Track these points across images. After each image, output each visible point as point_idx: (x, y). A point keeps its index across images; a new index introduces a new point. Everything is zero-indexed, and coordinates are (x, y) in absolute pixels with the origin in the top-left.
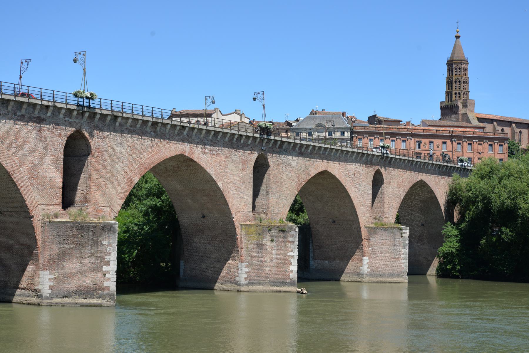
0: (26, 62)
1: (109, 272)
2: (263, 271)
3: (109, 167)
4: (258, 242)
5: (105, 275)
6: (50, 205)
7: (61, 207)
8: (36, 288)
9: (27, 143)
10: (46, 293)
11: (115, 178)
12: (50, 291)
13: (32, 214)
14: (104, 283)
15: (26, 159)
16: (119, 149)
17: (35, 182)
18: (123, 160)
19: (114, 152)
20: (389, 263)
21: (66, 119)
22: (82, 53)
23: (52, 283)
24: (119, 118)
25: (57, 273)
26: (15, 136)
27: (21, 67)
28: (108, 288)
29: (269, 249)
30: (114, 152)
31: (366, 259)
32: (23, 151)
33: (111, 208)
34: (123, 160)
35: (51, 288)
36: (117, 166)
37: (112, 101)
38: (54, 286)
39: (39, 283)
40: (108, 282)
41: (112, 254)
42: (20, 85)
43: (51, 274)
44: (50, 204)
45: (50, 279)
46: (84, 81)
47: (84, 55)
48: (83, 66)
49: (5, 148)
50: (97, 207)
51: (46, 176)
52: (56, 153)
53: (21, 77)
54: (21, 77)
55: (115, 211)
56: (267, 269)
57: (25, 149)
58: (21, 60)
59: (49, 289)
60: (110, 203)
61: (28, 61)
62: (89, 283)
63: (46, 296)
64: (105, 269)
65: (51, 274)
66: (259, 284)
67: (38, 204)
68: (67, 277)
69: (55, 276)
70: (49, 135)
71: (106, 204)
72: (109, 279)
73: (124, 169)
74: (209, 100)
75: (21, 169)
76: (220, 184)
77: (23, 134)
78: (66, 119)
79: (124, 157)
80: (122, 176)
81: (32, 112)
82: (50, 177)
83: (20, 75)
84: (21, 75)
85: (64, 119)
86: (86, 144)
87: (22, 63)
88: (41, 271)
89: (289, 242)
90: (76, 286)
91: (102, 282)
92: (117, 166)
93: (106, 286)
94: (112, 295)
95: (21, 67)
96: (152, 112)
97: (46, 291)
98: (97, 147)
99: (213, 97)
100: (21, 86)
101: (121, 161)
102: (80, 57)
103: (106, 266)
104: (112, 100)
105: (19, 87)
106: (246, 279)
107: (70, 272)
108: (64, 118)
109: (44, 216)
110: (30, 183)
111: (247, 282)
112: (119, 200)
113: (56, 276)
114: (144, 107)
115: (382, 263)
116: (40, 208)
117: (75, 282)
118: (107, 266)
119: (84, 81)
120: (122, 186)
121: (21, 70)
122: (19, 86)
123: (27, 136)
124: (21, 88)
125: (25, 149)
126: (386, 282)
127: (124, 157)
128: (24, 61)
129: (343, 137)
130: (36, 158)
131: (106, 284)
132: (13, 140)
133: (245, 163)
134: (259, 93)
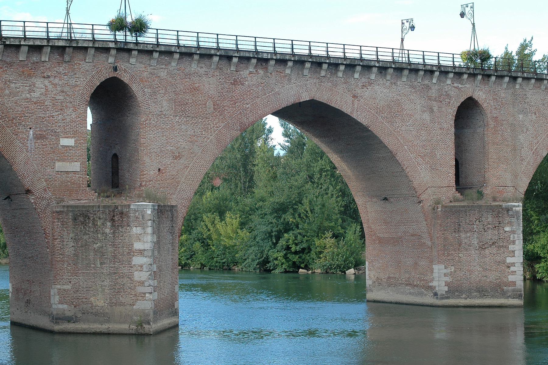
0: (407, 22)
1: (513, 264)
3: (511, 139)
6: (442, 187)
7: (454, 190)
8: (430, 284)
9: (411, 116)
10: (441, 290)
11: (518, 151)
12: (446, 289)
14: (509, 277)
15: (411, 135)
16: (521, 116)
17: (422, 161)
18: (527, 130)
19: (515, 120)
21: (456, 85)
22: (469, 6)
23: (448, 279)
24: (519, 79)
25: (453, 267)
26: (396, 109)
27: (402, 28)
28: (514, 283)
30: (515, 120)
32: (407, 125)
33: (515, 189)
34: (527, 130)
35: (447, 284)
36: (520, 137)
37: (438, 53)
38: (452, 282)
39: (432, 280)
40: (514, 276)
41: (517, 242)
42: (402, 50)
43: (446, 268)
44: (441, 186)
45: (445, 275)
46: (474, 37)
47: (472, 7)
48: (472, 20)
49: (386, 123)
50: (497, 187)
51: (435, 154)
52: (445, 126)
53: (402, 40)
54: (402, 40)
55: (520, 191)
57: (409, 123)
58: (402, 20)
59: (445, 286)
60: (513, 182)
61: (410, 20)
62: (492, 277)
63: (442, 294)
64: (509, 260)
65: (446, 268)
67: (428, 186)
68: (465, 271)
69: (451, 271)
70: (435, 105)
71: (509, 183)
72: (514, 272)
73: (529, 140)
74: (407, 25)
75: (406, 147)
77: (406, 106)
78: (456, 85)
79: (528, 125)
80: (526, 148)
81: (415, 79)
82: (440, 155)
83: (402, 38)
84: (403, 38)
85: (453, 85)
86: (481, 113)
87: (403, 23)
88: (435, 264)
90: (476, 282)
91: (506, 277)
92: (520, 137)
93: (511, 280)
95: (402, 28)
96: (424, 57)
98: (494, 116)
99: (412, 20)
100: (403, 50)
101: (525, 130)
102: (467, 10)
103: (510, 257)
104: (327, 43)
105: (401, 52)
107: (468, 265)
108: (453, 84)
110: (416, 163)
112: (524, 178)
113: (452, 271)
114: (159, 32)
116: (429, 191)
117: (474, 277)
118: (511, 257)
119: (474, 37)
120: (527, 160)
121: (402, 32)
122: (401, 50)
123: (410, 108)
124: (403, 52)
125: (409, 123)
126: (458, 307)
127: (528, 125)
128: (405, 21)
130: (422, 132)
131: (511, 278)
132: (394, 113)
134: (467, 6)
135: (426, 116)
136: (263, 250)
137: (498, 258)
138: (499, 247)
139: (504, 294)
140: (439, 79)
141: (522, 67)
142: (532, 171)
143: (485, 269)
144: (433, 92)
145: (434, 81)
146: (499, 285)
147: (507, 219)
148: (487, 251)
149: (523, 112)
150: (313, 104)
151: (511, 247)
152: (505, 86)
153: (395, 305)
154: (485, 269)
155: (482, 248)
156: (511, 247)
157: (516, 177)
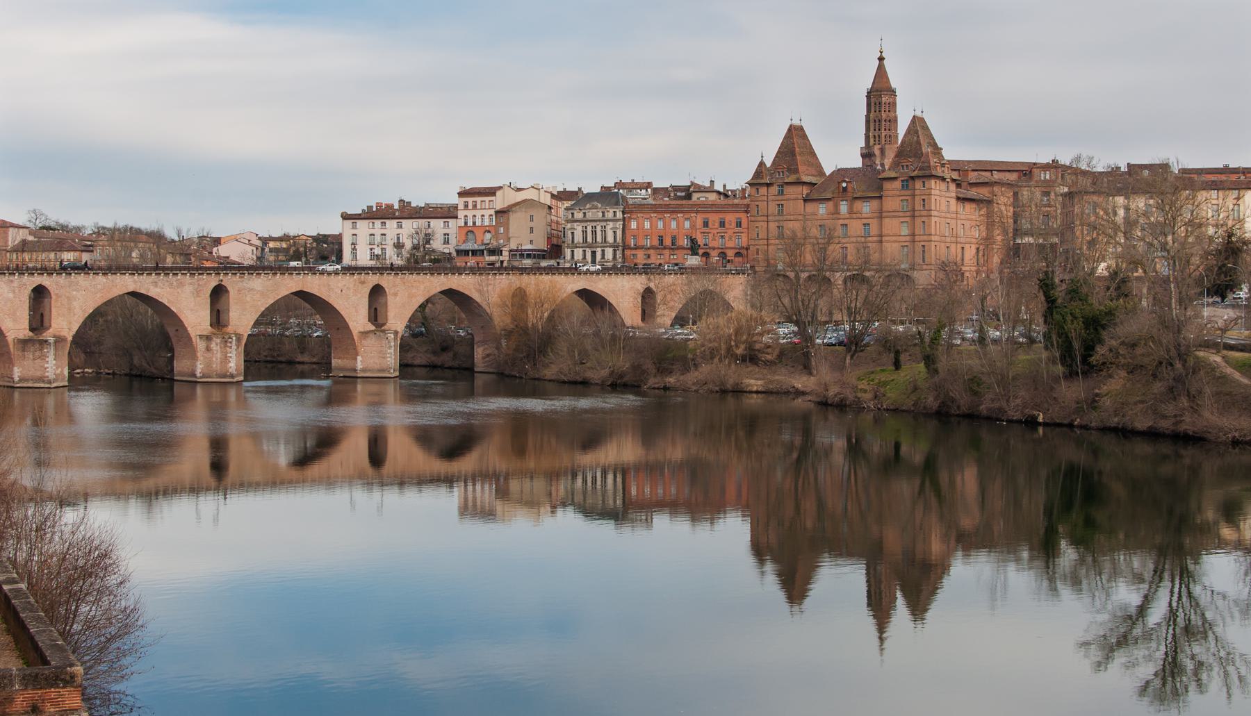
1: (48, 368)
2: (212, 367)
4: (207, 347)
5: (46, 369)
13: (7, 335)
20: (377, 361)
23: (19, 374)
29: (215, 352)
31: (359, 358)
35: (19, 377)
56: (214, 366)
62: (39, 374)
64: (46, 365)
66: (210, 377)
71: (65, 327)
76: (91, 311)
89: (228, 347)
94: (428, 415)
97: (16, 379)
106: (200, 373)
109: (1137, 313)
111: (201, 375)
115: (372, 361)
129: (722, 216)
131: (47, 374)
133: (197, 293)
135: (11, 295)
136: (1035, 390)
137: (42, 364)
138: (42, 359)
139: (43, 382)
140: (240, 277)
141: (914, 265)
142: (81, 320)
143: (36, 370)
144: (15, 284)
145: (16, 277)
146: (41, 378)
147: (45, 346)
148: (36, 361)
149: (77, 290)
150: (585, 290)
151: (47, 359)
152: (63, 278)
153: (55, 390)
154: (36, 370)
155: (34, 359)
156: (47, 359)
157: (70, 323)
